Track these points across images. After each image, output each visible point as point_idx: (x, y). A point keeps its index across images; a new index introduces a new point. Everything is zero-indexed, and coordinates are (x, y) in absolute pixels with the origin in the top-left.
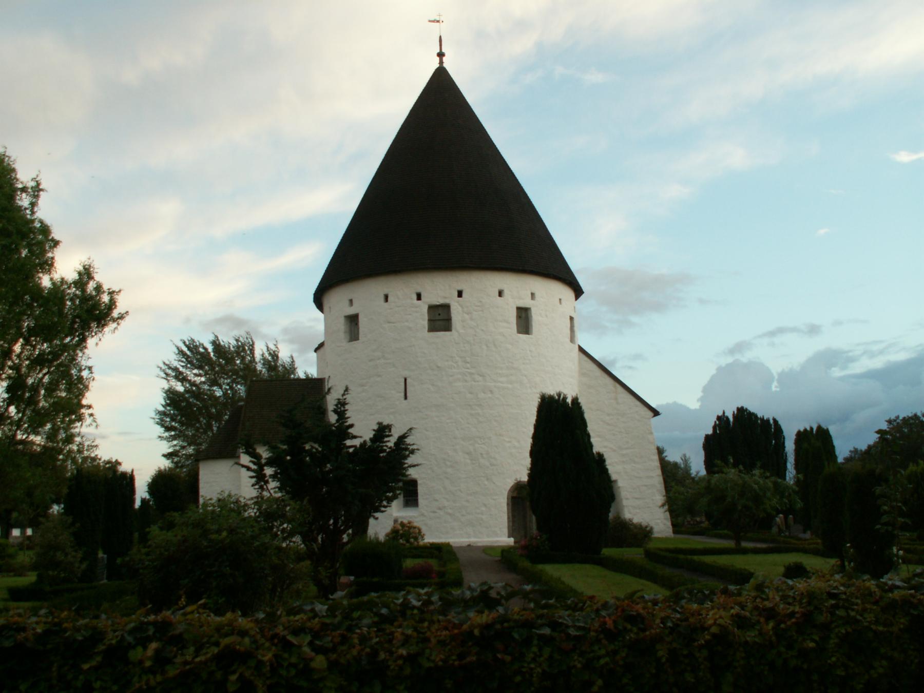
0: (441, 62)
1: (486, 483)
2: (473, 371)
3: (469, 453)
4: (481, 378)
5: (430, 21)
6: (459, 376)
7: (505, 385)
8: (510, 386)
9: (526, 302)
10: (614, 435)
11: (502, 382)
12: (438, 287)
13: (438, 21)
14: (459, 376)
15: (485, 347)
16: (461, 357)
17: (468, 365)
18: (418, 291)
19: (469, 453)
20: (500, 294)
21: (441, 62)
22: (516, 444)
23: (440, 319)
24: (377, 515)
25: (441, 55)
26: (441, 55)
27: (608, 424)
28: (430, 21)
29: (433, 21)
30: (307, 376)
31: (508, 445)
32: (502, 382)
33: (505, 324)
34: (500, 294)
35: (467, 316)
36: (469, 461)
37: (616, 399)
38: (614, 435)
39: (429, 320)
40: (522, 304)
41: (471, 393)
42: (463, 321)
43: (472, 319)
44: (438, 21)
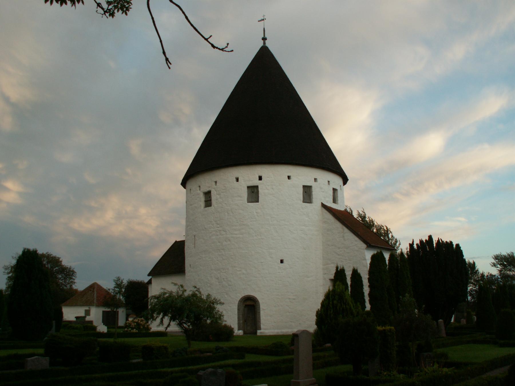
0: (264, 43)
1: (226, 296)
2: (220, 229)
3: (218, 279)
4: (224, 233)
5: (259, 21)
6: (214, 233)
7: (237, 236)
8: (241, 236)
9: (255, 182)
10: (342, 261)
11: (236, 234)
12: (248, 175)
13: (263, 20)
14: (214, 233)
15: (226, 214)
16: (215, 221)
17: (218, 226)
18: (260, 175)
19: (218, 279)
20: (237, 180)
21: (264, 43)
22: (244, 272)
23: (253, 193)
24: (231, 317)
25: (264, 39)
26: (264, 39)
27: (339, 255)
28: (259, 21)
29: (261, 21)
30: (364, 217)
31: (238, 273)
32: (236, 234)
33: (240, 198)
34: (237, 180)
35: (218, 196)
36: (217, 283)
37: (343, 237)
38: (342, 261)
39: (205, 201)
40: (251, 184)
41: (219, 242)
42: (217, 199)
43: (221, 198)
44: (263, 20)
